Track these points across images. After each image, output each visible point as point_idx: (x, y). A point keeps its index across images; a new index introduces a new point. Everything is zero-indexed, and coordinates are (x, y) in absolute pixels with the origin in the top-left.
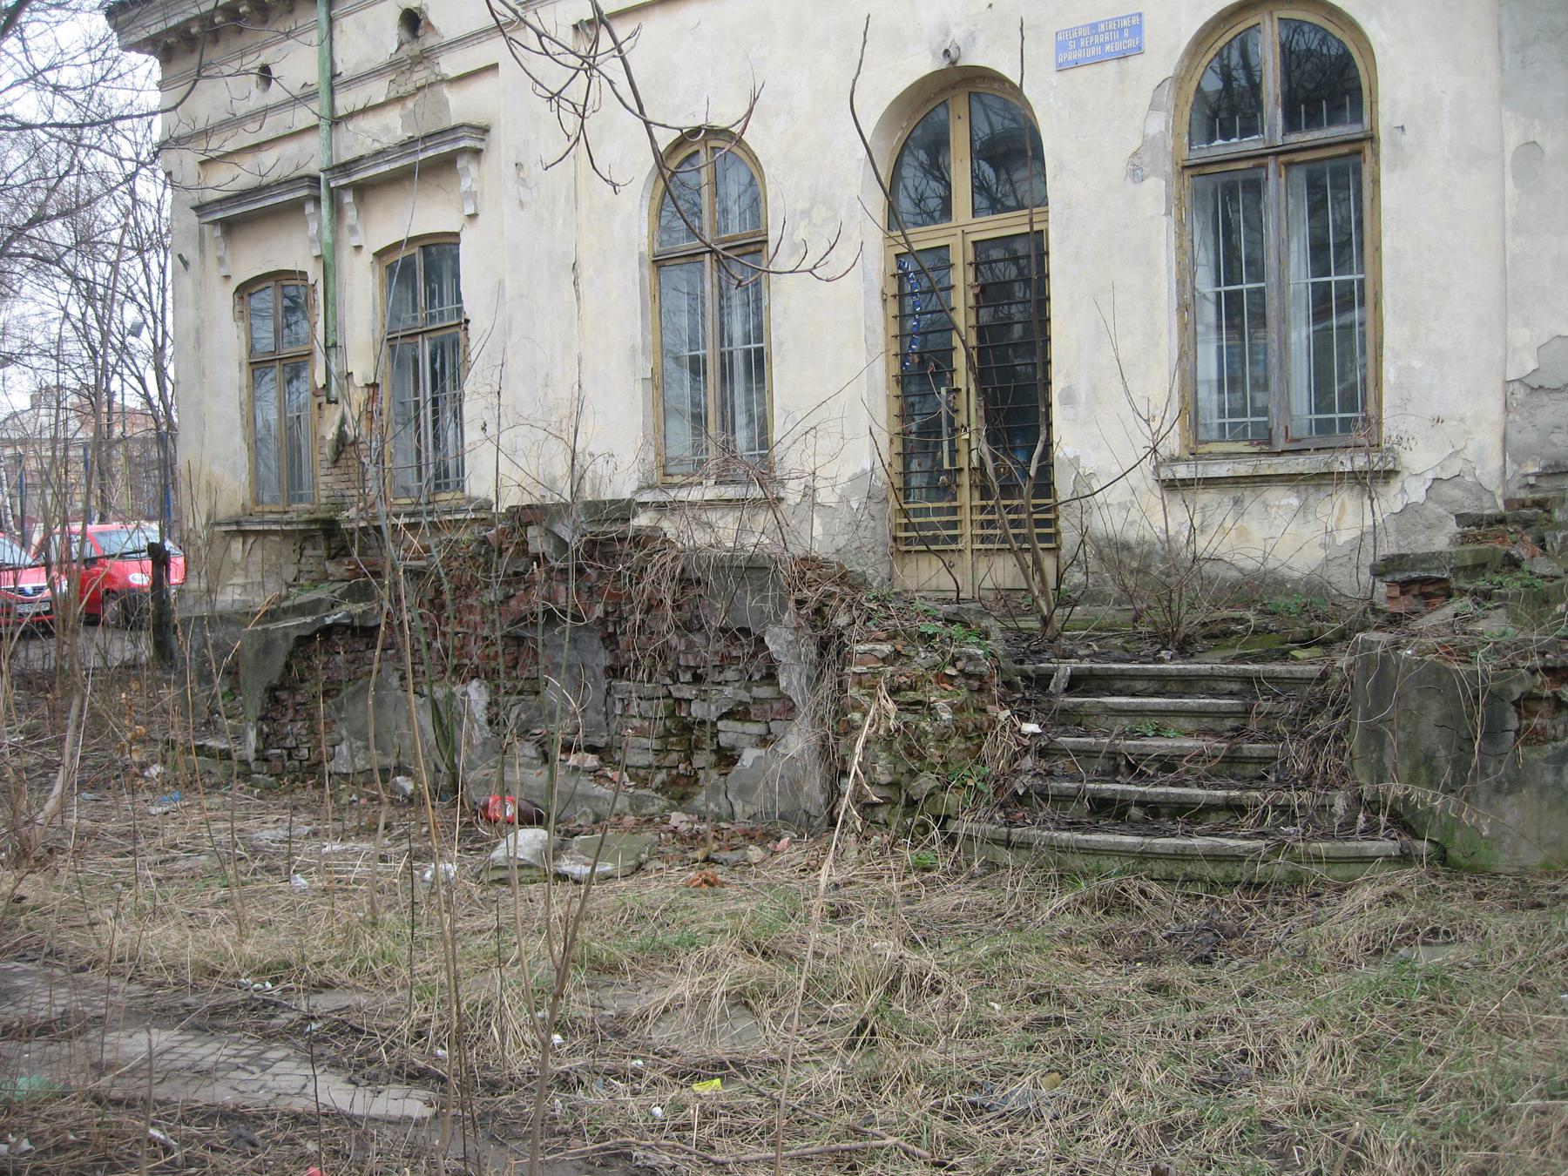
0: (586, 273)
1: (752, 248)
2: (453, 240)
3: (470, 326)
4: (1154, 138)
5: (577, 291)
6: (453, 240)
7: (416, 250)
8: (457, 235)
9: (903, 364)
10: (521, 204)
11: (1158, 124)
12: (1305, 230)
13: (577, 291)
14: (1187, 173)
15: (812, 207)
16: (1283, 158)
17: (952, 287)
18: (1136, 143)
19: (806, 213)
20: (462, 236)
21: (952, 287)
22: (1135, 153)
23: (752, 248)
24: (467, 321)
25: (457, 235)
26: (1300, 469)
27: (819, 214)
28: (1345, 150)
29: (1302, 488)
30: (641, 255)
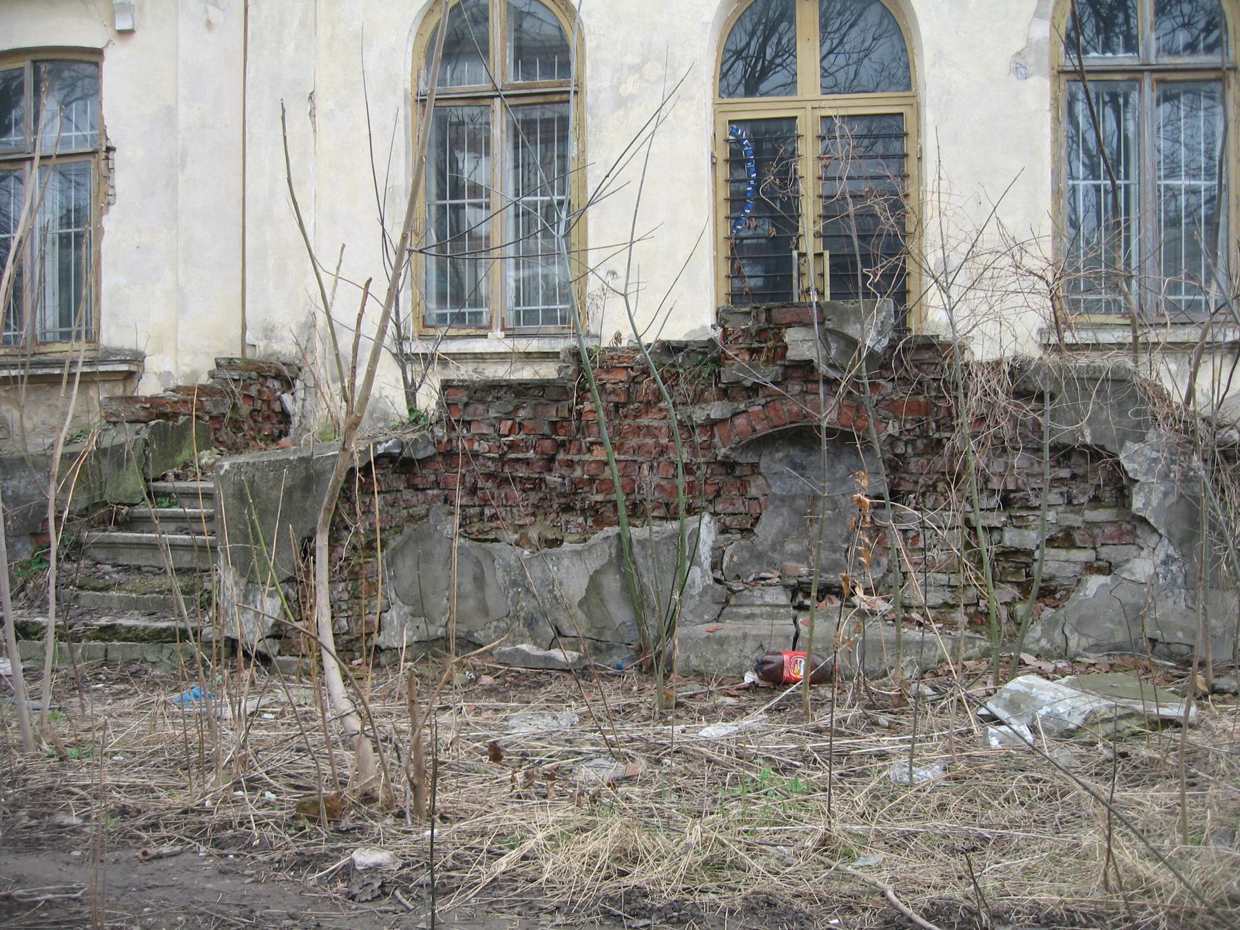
0: (323, 105)
1: (557, 98)
2: (94, 58)
3: (115, 156)
4: (1038, 42)
5: (314, 123)
6: (94, 58)
7: (26, 64)
8: (99, 52)
9: (734, 227)
10: (209, 25)
11: (1042, 31)
12: (372, 391)
13: (314, 123)
14: (1063, 78)
15: (644, 63)
16: (1156, 76)
17: (906, 134)
18: (1019, 45)
19: (636, 69)
20: (107, 53)
21: (906, 134)
22: (1019, 54)
23: (557, 98)
24: (109, 149)
25: (99, 52)
26: (1185, 339)
27: (654, 70)
28: (1212, 75)
29: (1179, 355)
30: (406, 90)
